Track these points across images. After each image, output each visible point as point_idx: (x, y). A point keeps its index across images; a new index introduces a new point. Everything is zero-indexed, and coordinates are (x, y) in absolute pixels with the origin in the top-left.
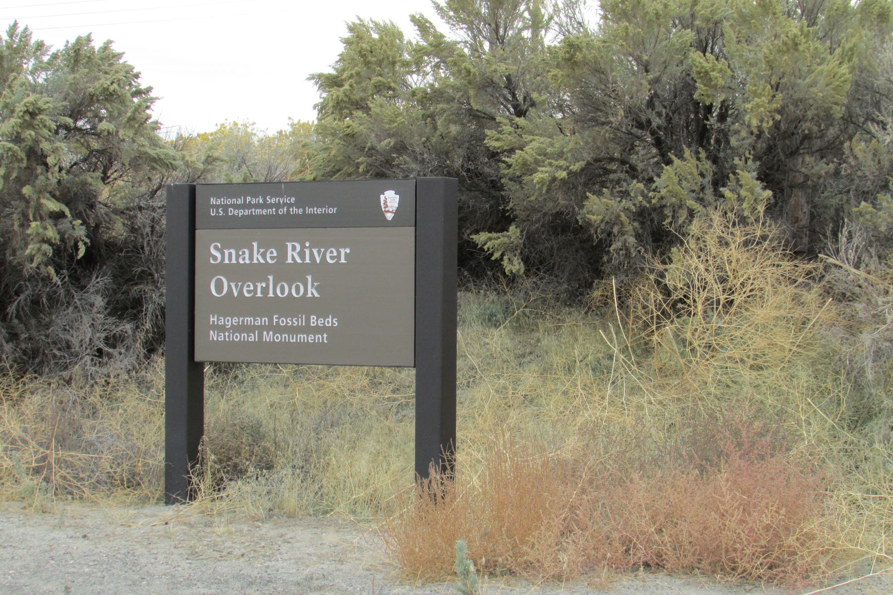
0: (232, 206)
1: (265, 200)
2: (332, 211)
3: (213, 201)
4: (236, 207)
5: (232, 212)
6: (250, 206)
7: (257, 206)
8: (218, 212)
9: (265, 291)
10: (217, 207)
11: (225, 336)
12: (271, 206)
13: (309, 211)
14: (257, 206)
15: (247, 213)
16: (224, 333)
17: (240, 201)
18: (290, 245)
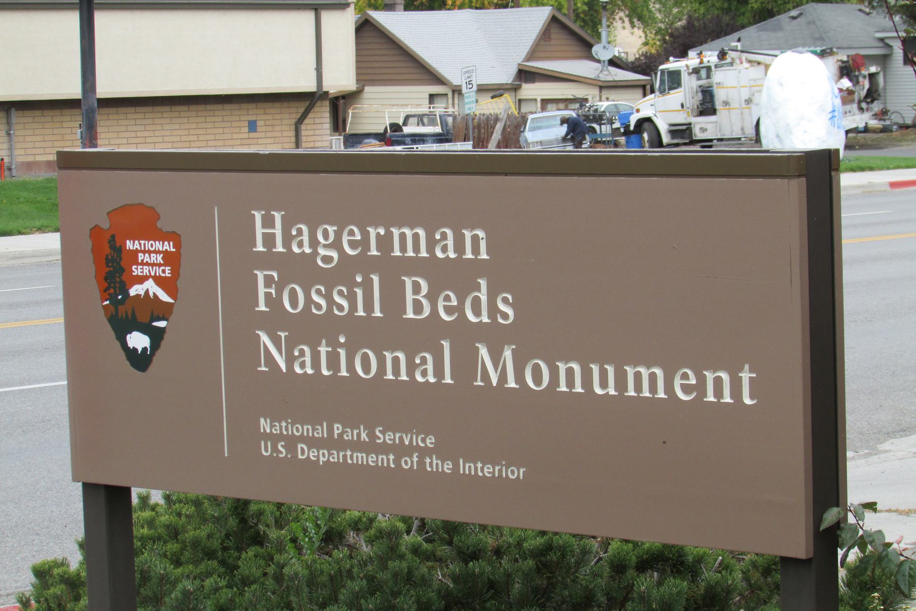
0: (302, 439)
1: (372, 435)
2: (516, 473)
3: (265, 425)
4: (313, 443)
5: (304, 452)
6: (340, 444)
7: (357, 446)
8: (275, 449)
9: (359, 435)
10: (274, 439)
11: (281, 427)
12: (384, 449)
13: (466, 468)
14: (357, 446)
15: (336, 457)
16: (280, 422)
17: (321, 432)
18: (408, 282)
